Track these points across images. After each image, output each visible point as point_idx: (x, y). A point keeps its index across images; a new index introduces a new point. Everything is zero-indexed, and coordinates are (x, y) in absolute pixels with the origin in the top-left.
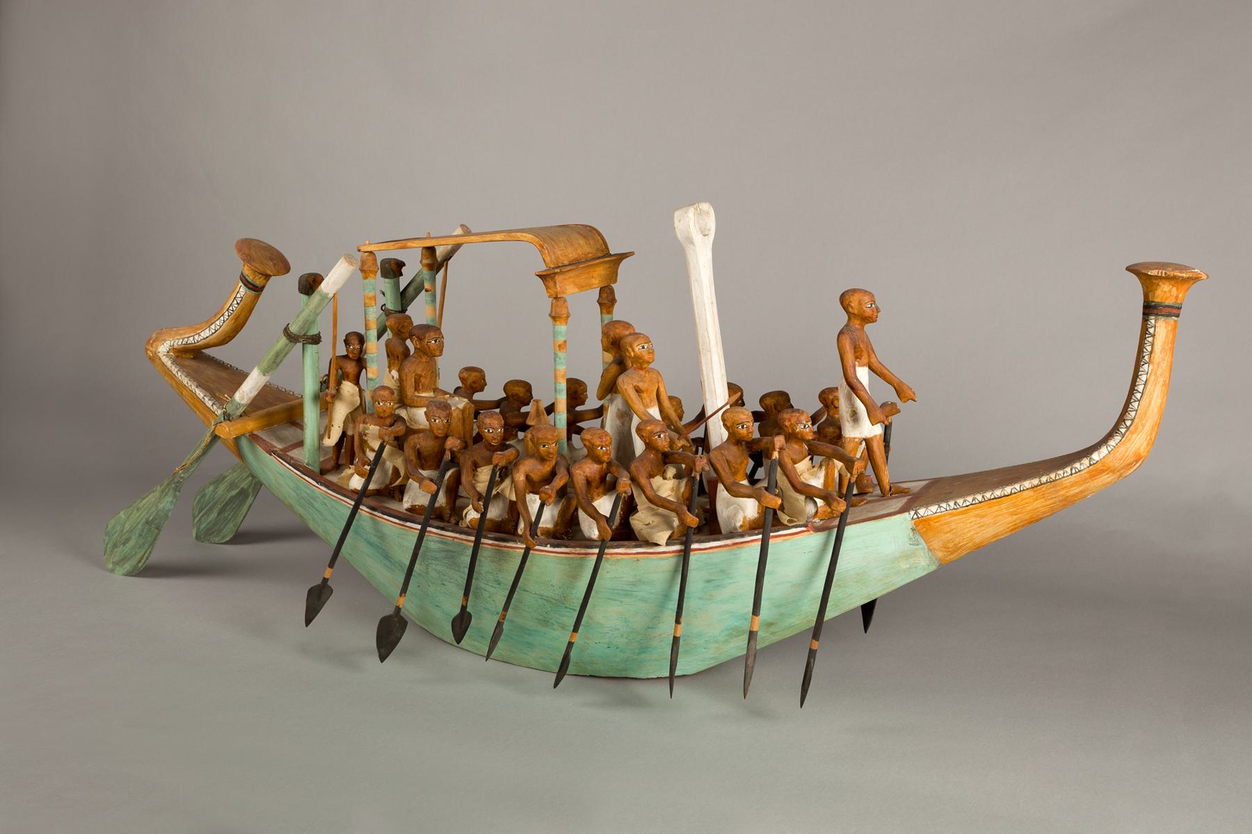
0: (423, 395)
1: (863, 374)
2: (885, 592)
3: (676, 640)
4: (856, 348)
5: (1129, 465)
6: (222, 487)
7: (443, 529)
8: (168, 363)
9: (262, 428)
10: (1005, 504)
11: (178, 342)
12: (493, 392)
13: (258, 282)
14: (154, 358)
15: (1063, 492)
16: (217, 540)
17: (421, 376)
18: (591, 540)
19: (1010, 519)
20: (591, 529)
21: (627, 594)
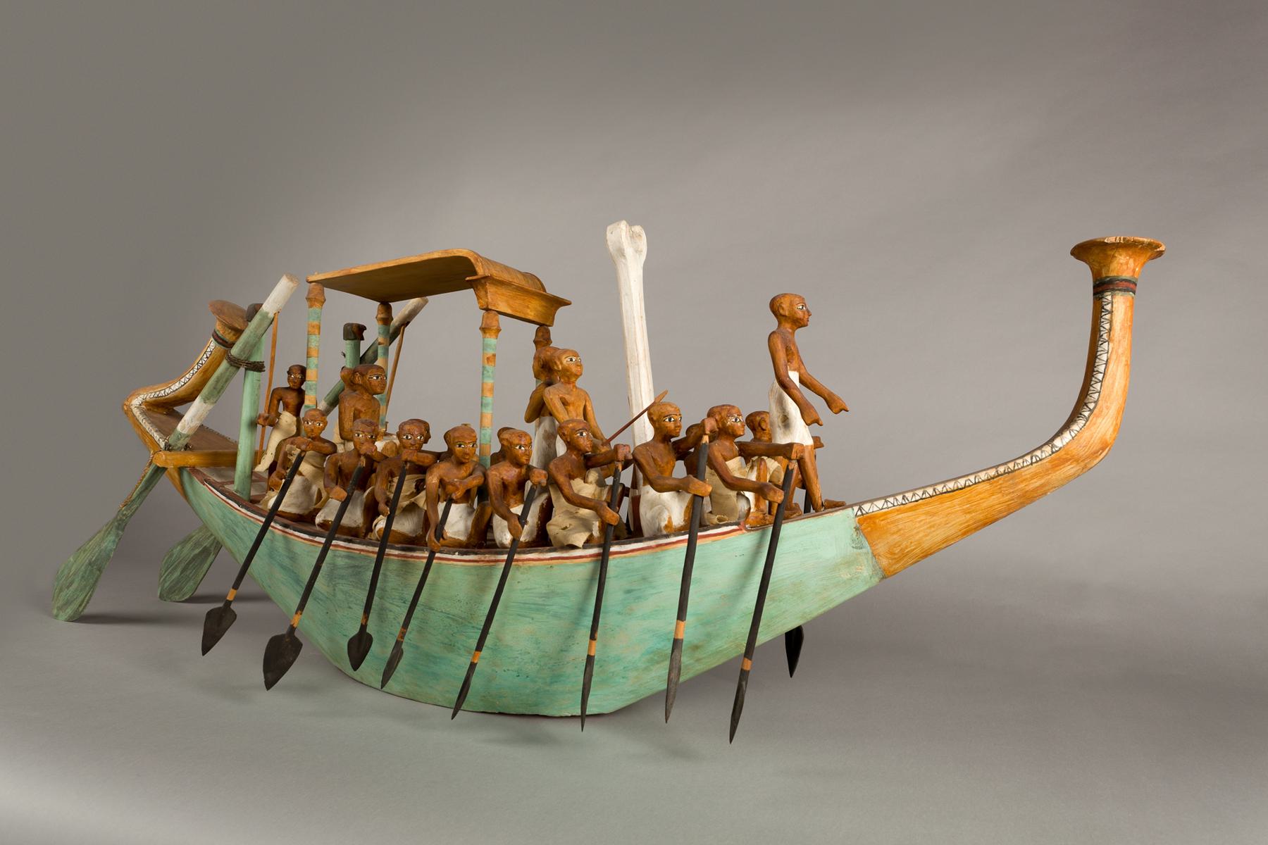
1: (794, 376)
2: (821, 611)
3: (590, 660)
4: (788, 350)
5: (1095, 454)
6: (189, 546)
7: (350, 541)
8: (140, 418)
9: (207, 466)
10: (959, 499)
11: (150, 395)
13: (229, 337)
14: (128, 412)
15: (1022, 485)
18: (503, 546)
19: (963, 518)
20: (504, 536)
21: (540, 608)
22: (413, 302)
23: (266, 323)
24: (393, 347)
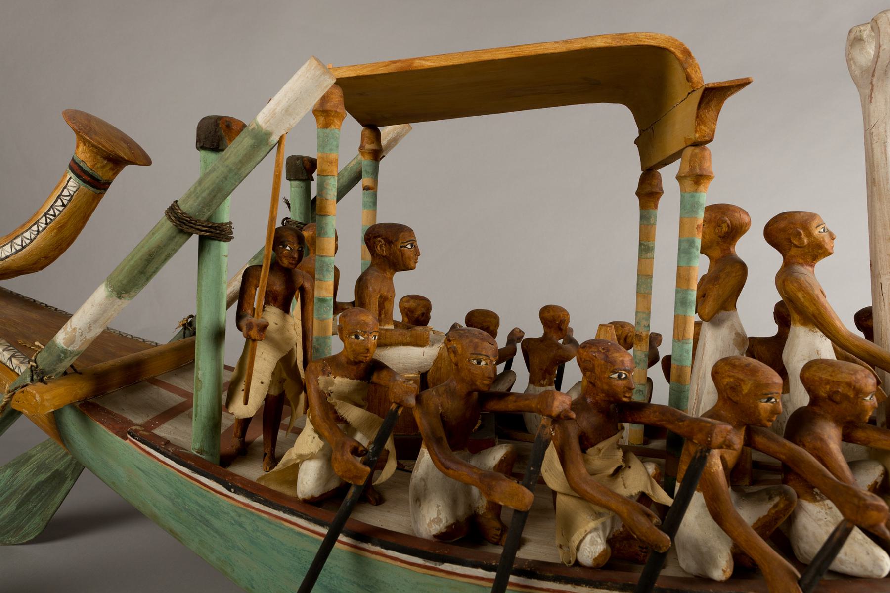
13: (100, 174)
16: (14, 540)
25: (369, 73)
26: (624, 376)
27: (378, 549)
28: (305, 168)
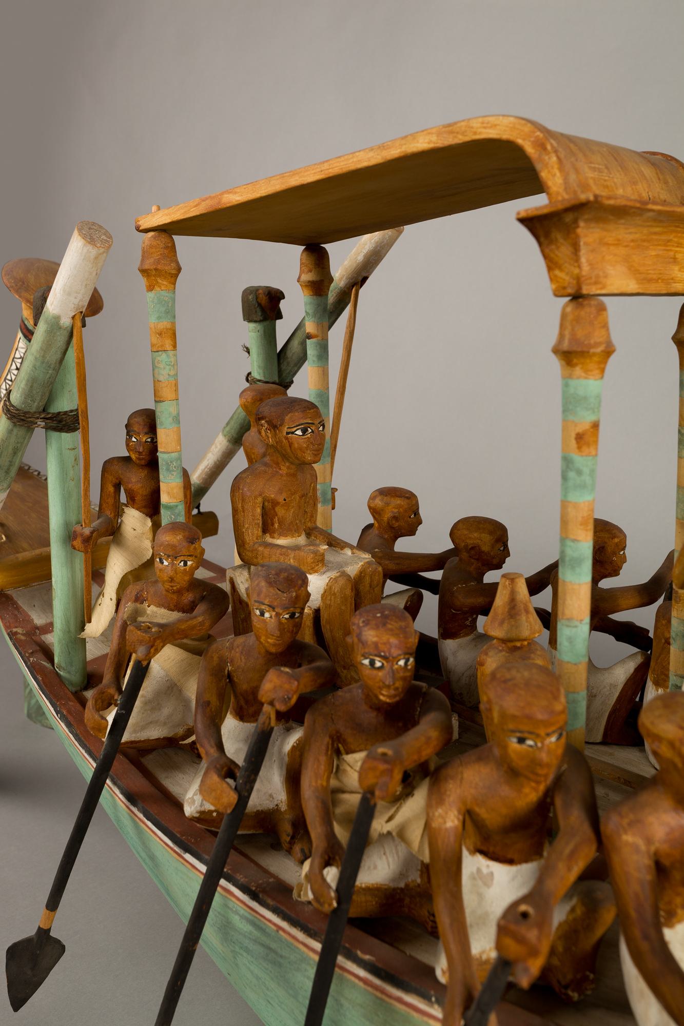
0: (281, 541)
12: (431, 539)
17: (275, 503)
22: (365, 242)
23: (61, 340)
24: (337, 333)
25: (182, 217)
26: (378, 664)
27: (141, 816)
28: (259, 305)
